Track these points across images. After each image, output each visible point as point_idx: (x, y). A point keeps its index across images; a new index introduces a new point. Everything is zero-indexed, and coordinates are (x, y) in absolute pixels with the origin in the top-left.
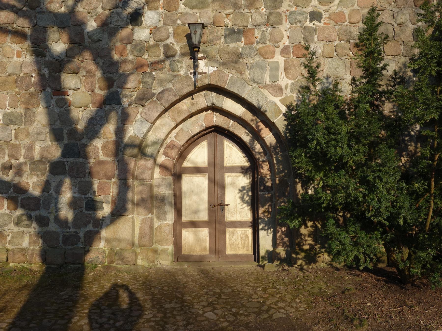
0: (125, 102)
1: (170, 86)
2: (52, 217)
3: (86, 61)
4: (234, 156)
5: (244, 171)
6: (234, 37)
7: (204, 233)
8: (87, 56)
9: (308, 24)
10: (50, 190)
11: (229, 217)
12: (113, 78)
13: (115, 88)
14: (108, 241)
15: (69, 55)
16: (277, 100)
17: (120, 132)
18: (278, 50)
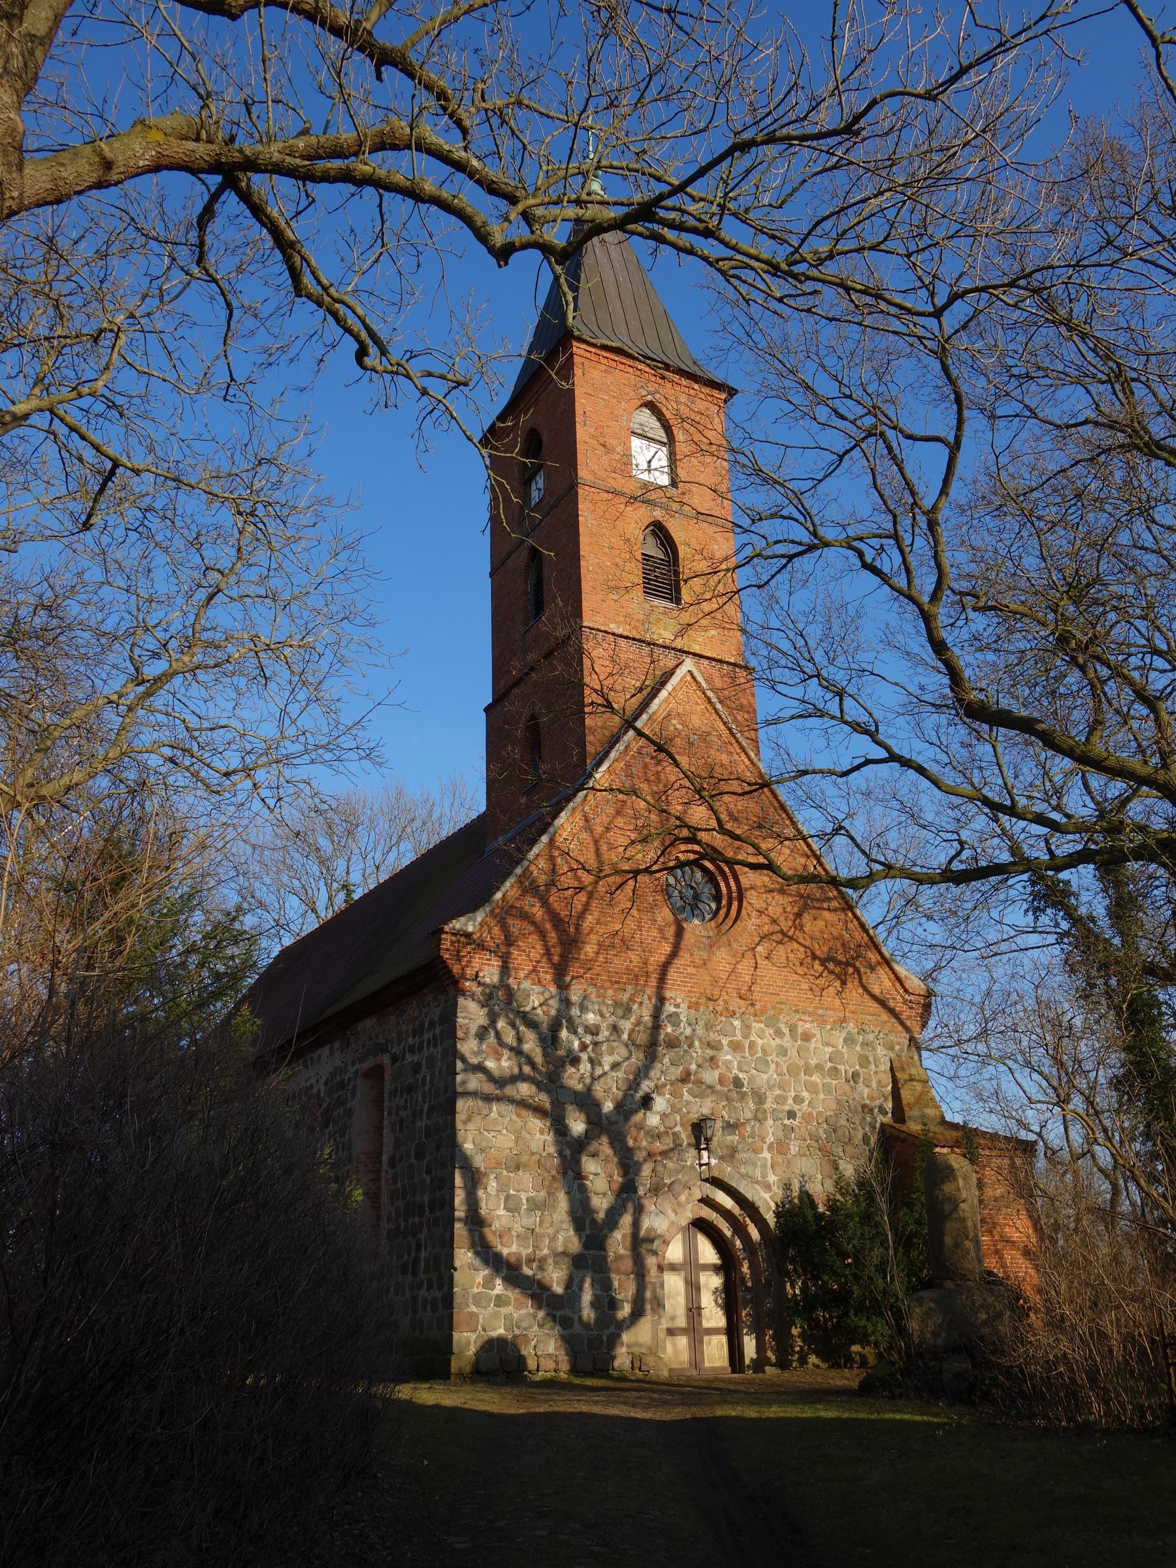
0: (641, 1192)
1: (680, 1176)
2: (576, 1318)
3: (604, 1146)
4: (708, 1253)
5: (716, 1269)
6: (730, 1130)
7: (683, 1341)
8: (605, 1140)
9: (786, 1122)
10: (573, 1285)
11: (706, 1324)
12: (628, 1165)
13: (631, 1176)
14: (628, 1346)
15: (588, 1136)
16: (767, 1196)
17: (636, 1225)
18: (765, 1147)
